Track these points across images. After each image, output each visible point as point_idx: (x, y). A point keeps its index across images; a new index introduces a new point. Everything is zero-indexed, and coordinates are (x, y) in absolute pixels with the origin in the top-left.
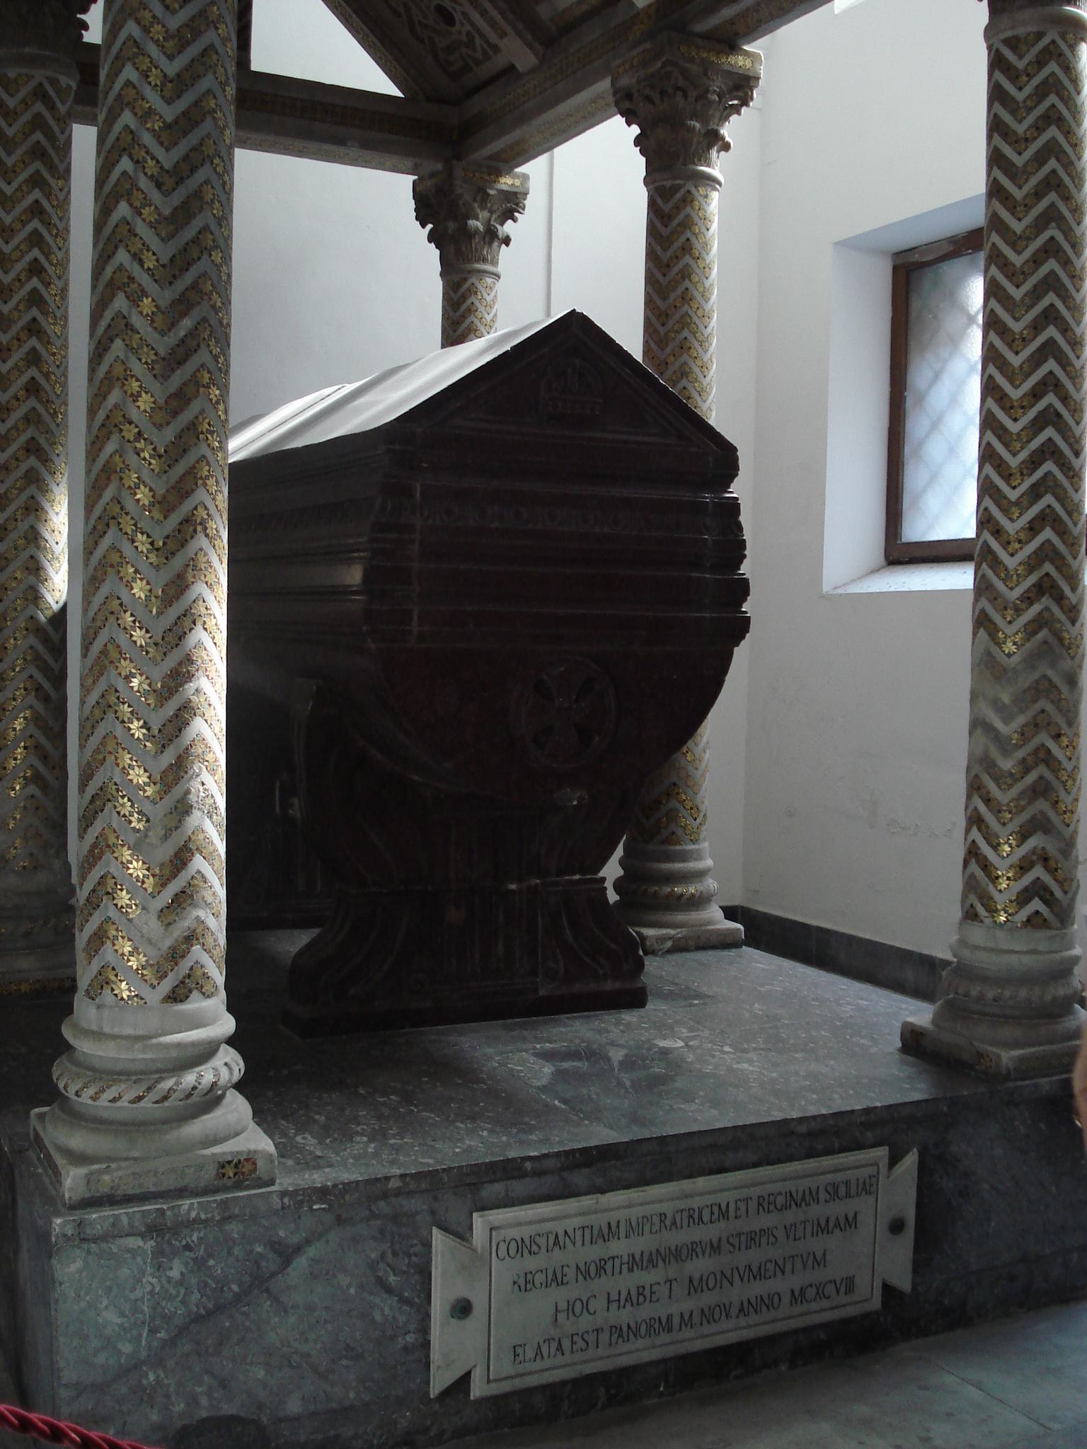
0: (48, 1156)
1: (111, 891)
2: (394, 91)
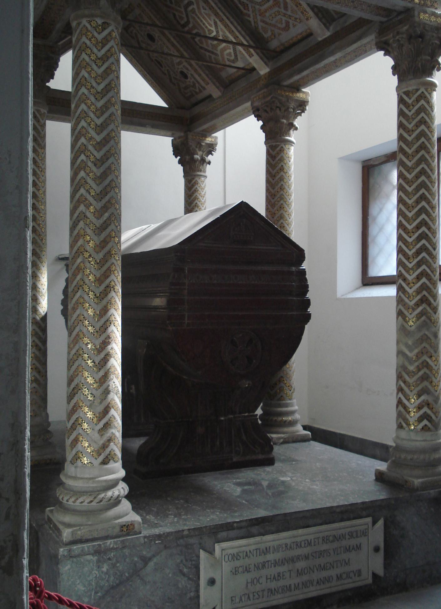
0: (55, 526)
1: (80, 423)
2: (164, 104)
